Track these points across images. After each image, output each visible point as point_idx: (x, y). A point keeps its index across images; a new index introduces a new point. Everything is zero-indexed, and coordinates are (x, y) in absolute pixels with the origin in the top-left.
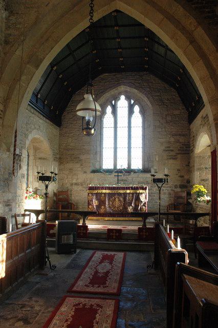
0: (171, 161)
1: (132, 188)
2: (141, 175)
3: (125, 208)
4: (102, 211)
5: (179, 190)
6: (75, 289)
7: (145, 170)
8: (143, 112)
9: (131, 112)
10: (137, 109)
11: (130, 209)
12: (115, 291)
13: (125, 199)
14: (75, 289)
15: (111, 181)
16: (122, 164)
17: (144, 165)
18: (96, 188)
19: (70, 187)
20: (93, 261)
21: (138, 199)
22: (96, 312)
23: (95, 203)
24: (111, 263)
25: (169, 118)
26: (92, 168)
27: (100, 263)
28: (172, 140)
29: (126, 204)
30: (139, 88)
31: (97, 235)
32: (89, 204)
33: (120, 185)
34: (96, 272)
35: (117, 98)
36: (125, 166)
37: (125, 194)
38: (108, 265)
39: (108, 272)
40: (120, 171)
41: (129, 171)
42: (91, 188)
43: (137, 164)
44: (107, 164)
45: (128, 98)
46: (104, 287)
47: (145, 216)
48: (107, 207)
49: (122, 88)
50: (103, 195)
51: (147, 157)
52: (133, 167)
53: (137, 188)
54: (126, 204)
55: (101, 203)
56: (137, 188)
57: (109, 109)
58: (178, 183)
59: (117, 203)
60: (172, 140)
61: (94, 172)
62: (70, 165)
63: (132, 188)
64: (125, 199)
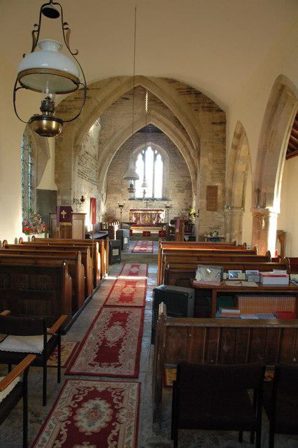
0: (181, 194)
1: (156, 210)
2: (161, 202)
3: (151, 221)
4: (138, 224)
5: (185, 212)
6: (73, 370)
7: (164, 199)
8: (163, 159)
9: (155, 159)
10: (159, 157)
11: (154, 222)
12: (132, 373)
13: (151, 216)
14: (73, 370)
15: (142, 205)
16: (149, 195)
17: (163, 196)
18: (135, 210)
19: (114, 209)
20: (99, 324)
21: (159, 217)
22: (128, 315)
23: (134, 219)
24: (123, 326)
25: (180, 166)
26: (129, 197)
27: (109, 326)
28: (181, 180)
29: (152, 219)
30: (156, 142)
31: (137, 235)
32: (130, 219)
33: (148, 208)
34: (105, 341)
35: (145, 149)
36: (151, 197)
37: (152, 214)
38: (119, 328)
39: (121, 340)
40: (147, 199)
41: (153, 199)
42: (131, 210)
43: (159, 195)
44: (138, 193)
45: (154, 149)
46: (116, 367)
47: (162, 225)
48: (141, 221)
49: (150, 143)
50: (74, 257)
51: (165, 190)
52: (155, 197)
53: (158, 210)
54: (152, 219)
55: (138, 219)
56: (158, 210)
57: (140, 156)
58: (184, 208)
59: (147, 219)
60: (181, 180)
61: (130, 199)
62: (115, 195)
63: (156, 210)
64: (151, 216)
